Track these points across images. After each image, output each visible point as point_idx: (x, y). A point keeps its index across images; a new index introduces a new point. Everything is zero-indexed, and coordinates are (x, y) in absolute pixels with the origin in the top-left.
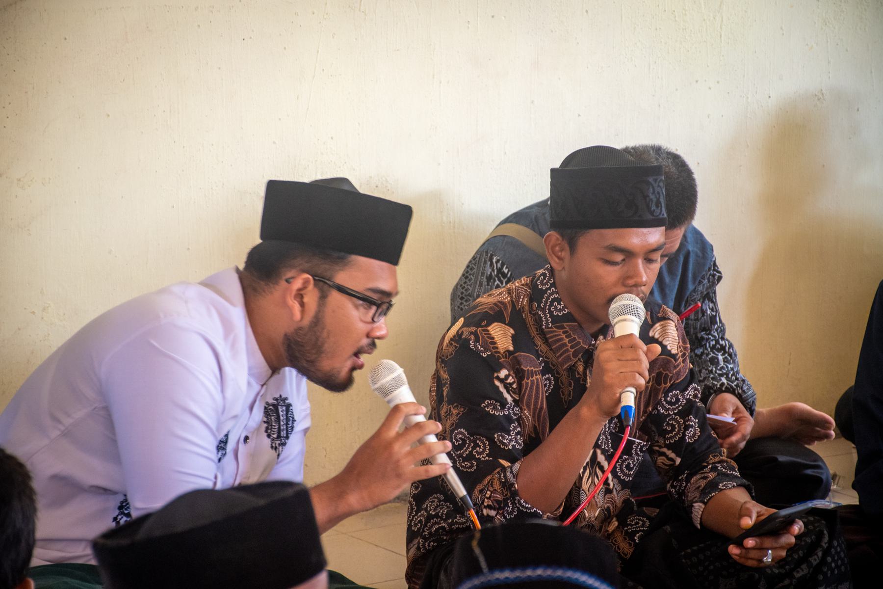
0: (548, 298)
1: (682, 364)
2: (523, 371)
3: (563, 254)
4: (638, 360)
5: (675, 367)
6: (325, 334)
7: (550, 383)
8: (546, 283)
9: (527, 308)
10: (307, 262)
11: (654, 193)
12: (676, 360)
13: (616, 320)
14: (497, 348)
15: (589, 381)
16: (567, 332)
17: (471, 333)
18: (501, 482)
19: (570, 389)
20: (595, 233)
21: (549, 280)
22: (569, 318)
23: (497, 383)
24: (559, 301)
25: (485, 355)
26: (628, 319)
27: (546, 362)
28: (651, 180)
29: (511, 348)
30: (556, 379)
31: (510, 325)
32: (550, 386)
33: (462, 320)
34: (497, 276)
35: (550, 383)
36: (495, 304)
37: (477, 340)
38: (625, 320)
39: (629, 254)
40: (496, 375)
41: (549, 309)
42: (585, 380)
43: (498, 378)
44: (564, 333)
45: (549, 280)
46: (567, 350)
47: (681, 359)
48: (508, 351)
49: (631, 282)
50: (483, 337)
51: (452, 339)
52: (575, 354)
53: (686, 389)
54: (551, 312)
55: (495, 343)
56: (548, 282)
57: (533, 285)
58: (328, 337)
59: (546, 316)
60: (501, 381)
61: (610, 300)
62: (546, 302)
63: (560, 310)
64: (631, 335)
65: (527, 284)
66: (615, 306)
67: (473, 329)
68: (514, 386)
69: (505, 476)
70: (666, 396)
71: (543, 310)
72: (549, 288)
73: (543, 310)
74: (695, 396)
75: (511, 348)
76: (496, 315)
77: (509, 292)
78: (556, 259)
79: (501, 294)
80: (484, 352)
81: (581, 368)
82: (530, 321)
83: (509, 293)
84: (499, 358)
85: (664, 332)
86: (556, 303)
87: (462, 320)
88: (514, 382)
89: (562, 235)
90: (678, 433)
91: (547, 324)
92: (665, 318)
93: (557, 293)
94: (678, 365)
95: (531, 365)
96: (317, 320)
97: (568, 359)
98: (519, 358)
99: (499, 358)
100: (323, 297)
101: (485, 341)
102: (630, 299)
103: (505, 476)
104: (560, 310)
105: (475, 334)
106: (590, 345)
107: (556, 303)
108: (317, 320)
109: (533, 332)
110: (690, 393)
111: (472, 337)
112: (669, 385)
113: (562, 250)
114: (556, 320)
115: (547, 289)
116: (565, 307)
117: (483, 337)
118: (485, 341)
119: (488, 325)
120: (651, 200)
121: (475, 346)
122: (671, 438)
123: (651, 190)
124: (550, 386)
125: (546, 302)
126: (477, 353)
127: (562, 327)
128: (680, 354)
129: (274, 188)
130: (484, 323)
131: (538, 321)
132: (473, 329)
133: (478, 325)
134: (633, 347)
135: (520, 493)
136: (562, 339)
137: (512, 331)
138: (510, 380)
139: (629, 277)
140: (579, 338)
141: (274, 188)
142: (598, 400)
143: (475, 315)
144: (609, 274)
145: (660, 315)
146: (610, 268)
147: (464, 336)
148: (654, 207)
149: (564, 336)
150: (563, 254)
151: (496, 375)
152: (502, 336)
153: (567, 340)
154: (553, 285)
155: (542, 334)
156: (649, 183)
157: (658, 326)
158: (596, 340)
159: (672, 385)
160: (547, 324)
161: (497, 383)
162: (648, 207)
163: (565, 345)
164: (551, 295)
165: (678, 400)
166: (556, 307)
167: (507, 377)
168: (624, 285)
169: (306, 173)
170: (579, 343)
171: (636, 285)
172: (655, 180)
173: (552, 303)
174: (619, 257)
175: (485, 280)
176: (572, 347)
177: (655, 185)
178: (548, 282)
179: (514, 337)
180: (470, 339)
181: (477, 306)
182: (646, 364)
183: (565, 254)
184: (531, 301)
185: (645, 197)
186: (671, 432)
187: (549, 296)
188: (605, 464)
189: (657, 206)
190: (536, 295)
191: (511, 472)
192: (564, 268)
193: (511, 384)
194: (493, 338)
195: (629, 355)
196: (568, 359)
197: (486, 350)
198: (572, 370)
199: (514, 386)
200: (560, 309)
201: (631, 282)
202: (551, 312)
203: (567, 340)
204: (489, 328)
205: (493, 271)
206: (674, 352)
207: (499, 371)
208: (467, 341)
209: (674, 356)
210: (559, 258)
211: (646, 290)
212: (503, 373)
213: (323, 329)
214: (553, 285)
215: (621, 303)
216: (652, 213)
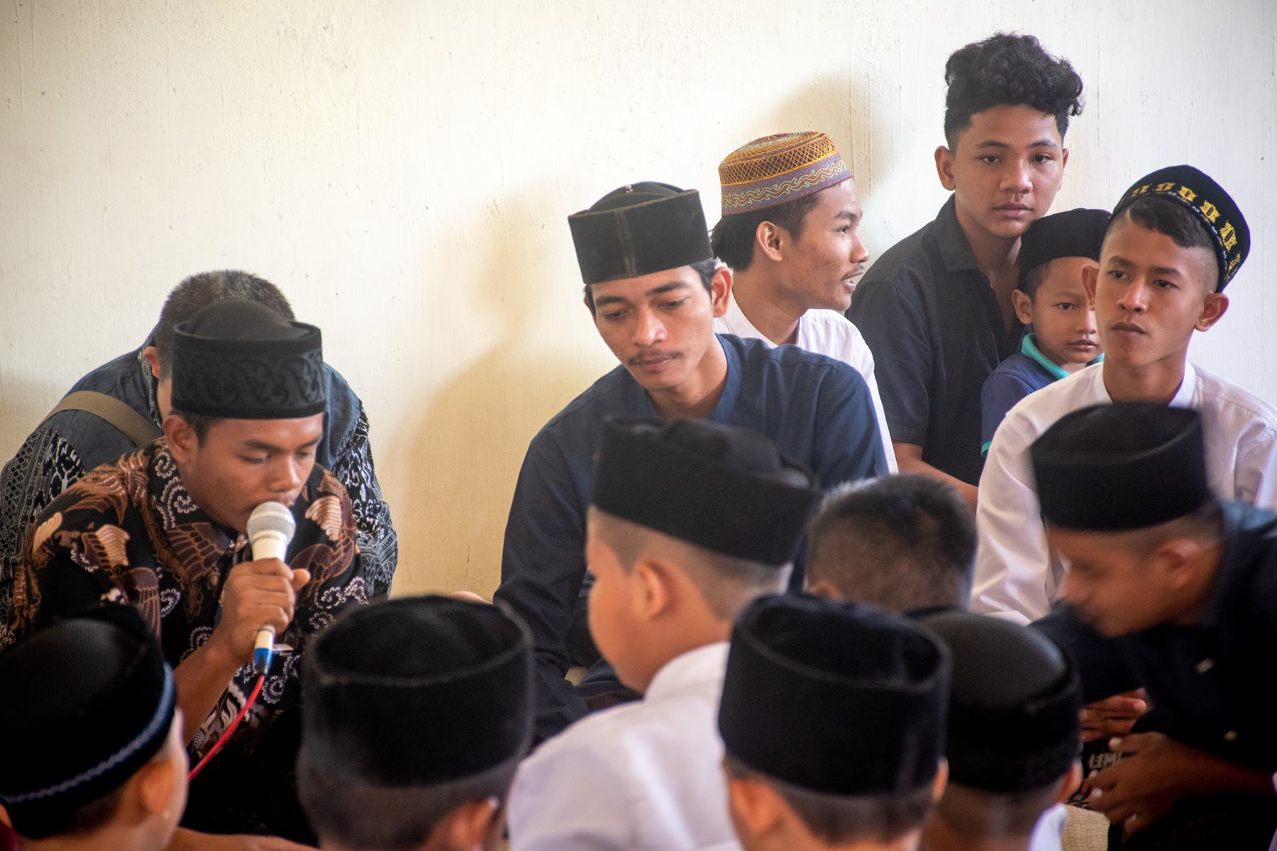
0: (170, 490)
2: (137, 592)
4: (283, 591)
5: (334, 558)
8: (167, 471)
9: (144, 503)
11: (309, 372)
12: (335, 549)
13: (255, 537)
14: (107, 561)
15: (223, 596)
17: (73, 540)
20: (232, 424)
21: (171, 466)
25: (91, 570)
26: (272, 537)
28: (306, 356)
29: (126, 563)
31: (124, 527)
34: (58, 465)
36: (105, 499)
37: (81, 549)
38: (268, 537)
39: (275, 452)
40: (103, 597)
41: (172, 505)
44: (193, 535)
45: (171, 466)
46: (197, 558)
47: (343, 547)
48: (122, 566)
49: (276, 485)
53: (347, 584)
54: (174, 510)
55: (105, 555)
61: (251, 508)
62: (168, 495)
63: (186, 507)
64: (274, 560)
66: (255, 517)
67: (76, 534)
70: (321, 594)
71: (164, 505)
72: (171, 478)
73: (164, 505)
74: (358, 592)
75: (126, 563)
76: (107, 514)
77: (123, 479)
79: (112, 482)
80: (90, 565)
81: (215, 580)
82: (149, 519)
83: (123, 484)
84: (110, 574)
85: (324, 512)
86: (180, 498)
89: (189, 421)
91: (170, 524)
92: (327, 493)
93: (181, 484)
95: (148, 579)
99: (110, 574)
101: (91, 551)
102: (278, 510)
104: (186, 507)
105: (79, 541)
106: (229, 549)
107: (180, 498)
109: (152, 534)
110: (352, 588)
111: (74, 545)
112: (322, 580)
113: (187, 438)
114: (181, 519)
115: (168, 479)
118: (91, 551)
119: (96, 528)
120: (306, 383)
121: (78, 557)
123: (306, 369)
126: (79, 568)
127: (190, 528)
130: (91, 526)
131: (159, 519)
134: (276, 573)
137: (126, 536)
139: (275, 480)
142: (230, 641)
144: (250, 475)
145: (320, 489)
146: (252, 468)
148: (308, 391)
149: (192, 540)
152: (110, 538)
153: (196, 545)
154: (176, 473)
155: (163, 535)
156: (303, 362)
157: (317, 504)
159: (327, 582)
160: (170, 524)
162: (303, 394)
163: (193, 551)
164: (174, 486)
165: (336, 599)
166: (180, 503)
168: (269, 490)
171: (284, 490)
172: (311, 356)
173: (175, 499)
174: (263, 455)
177: (311, 362)
179: (128, 544)
180: (71, 549)
182: (292, 598)
183: (192, 443)
184: (149, 494)
185: (298, 379)
188: (240, 696)
189: (313, 389)
192: (189, 461)
194: (102, 548)
195: (272, 582)
196: (198, 568)
197: (93, 563)
198: (204, 581)
200: (186, 506)
201: (276, 485)
202: (174, 510)
206: (335, 538)
207: (108, 591)
209: (332, 544)
210: (183, 447)
211: (293, 494)
214: (176, 473)
215: (264, 514)
216: (306, 398)
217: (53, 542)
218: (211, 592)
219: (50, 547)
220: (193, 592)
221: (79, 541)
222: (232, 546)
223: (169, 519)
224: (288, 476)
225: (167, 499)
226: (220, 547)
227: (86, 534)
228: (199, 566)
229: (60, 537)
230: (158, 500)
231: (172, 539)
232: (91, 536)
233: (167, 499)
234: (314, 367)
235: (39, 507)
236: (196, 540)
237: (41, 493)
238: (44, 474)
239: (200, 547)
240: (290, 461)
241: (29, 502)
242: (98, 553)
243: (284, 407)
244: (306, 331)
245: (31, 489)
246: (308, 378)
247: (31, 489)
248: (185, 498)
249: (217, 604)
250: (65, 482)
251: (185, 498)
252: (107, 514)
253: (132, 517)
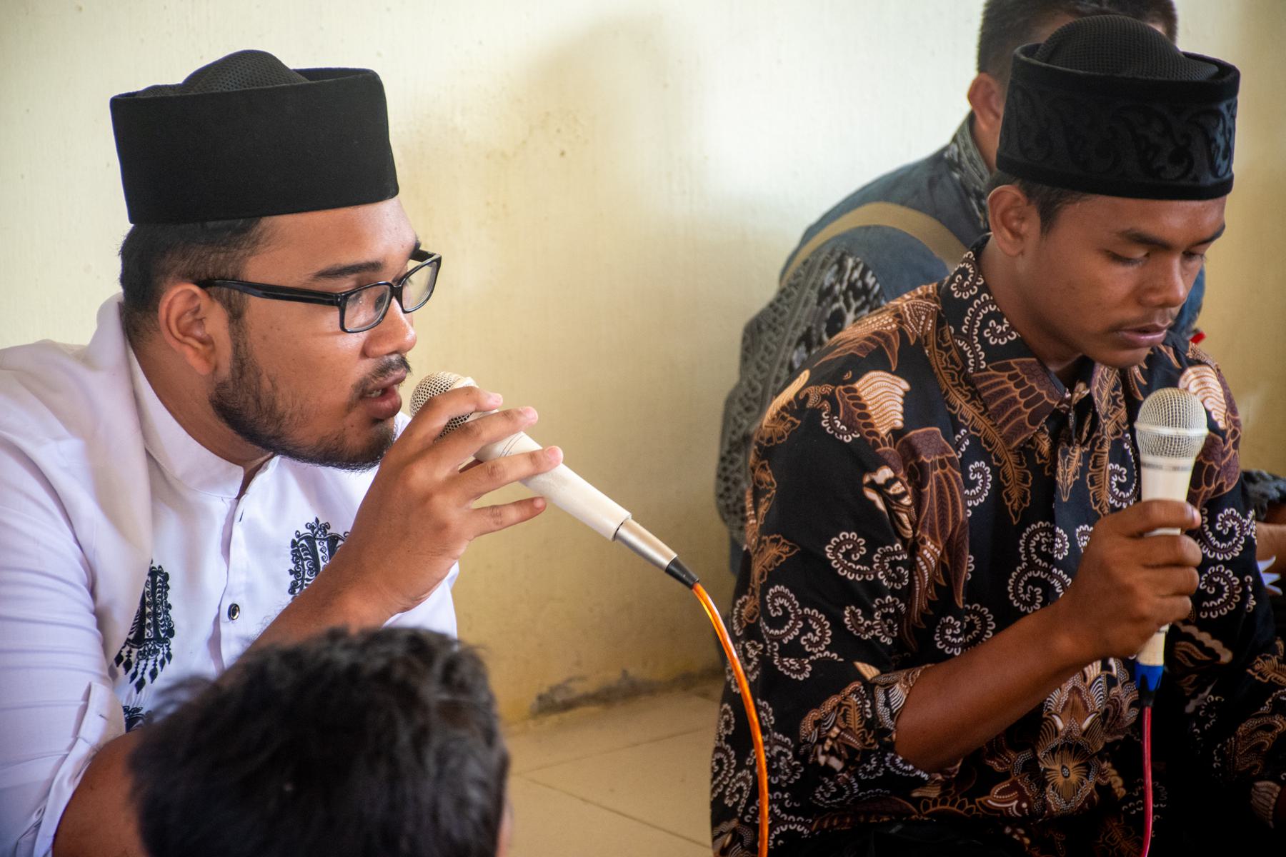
0: (975, 314)
1: (1232, 451)
3: (1024, 228)
6: (266, 384)
7: (985, 478)
8: (970, 287)
9: (932, 338)
10: (184, 257)
16: (1017, 376)
18: (863, 717)
19: (1025, 486)
21: (975, 280)
22: (1020, 348)
23: (871, 495)
24: (998, 317)
25: (848, 439)
27: (972, 438)
30: (995, 471)
32: (984, 484)
33: (805, 376)
34: (845, 293)
35: (985, 478)
36: (868, 339)
37: (834, 411)
40: (867, 479)
41: (980, 335)
42: (1053, 469)
43: (873, 485)
44: (1011, 378)
45: (975, 280)
46: (1018, 412)
47: (1231, 441)
50: (846, 405)
51: (783, 408)
52: (1034, 419)
54: (983, 341)
55: (868, 416)
56: (973, 283)
57: (944, 296)
58: (275, 388)
59: (973, 348)
60: (879, 489)
62: (972, 323)
65: (928, 296)
67: (827, 389)
68: (906, 501)
69: (873, 708)
71: (968, 338)
72: (978, 296)
76: (873, 356)
78: (1008, 235)
81: (1045, 446)
82: (938, 361)
86: (992, 323)
87: (805, 376)
88: (904, 494)
89: (1029, 194)
90: (1227, 602)
91: (977, 363)
93: (993, 303)
94: (1228, 451)
96: (242, 363)
97: (1021, 427)
98: (915, 441)
99: (876, 445)
100: (236, 316)
103: (873, 708)
105: (831, 398)
108: (242, 363)
109: (946, 381)
111: (826, 404)
113: (1022, 219)
114: (993, 354)
115: (972, 298)
116: (1012, 328)
117: (846, 405)
118: (849, 413)
119: (856, 378)
121: (831, 423)
122: (1213, 609)
124: (984, 484)
125: (972, 323)
127: (1007, 367)
128: (1230, 431)
129: (129, 112)
130: (848, 376)
132: (827, 389)
133: (836, 379)
135: (897, 748)
136: (1007, 390)
137: (906, 386)
138: (897, 488)
139: (1153, 290)
140: (1041, 387)
141: (129, 112)
143: (830, 363)
146: (1120, 270)
147: (809, 405)
148: (1219, 160)
149: (1011, 384)
150: (1024, 228)
151: (867, 479)
152: (884, 396)
153: (1016, 392)
154: (985, 288)
158: (1072, 392)
160: (977, 363)
161: (871, 495)
163: (1013, 401)
166: (993, 330)
167: (889, 482)
169: (171, 68)
170: (1040, 397)
174: (1139, 253)
175: (814, 296)
176: (1027, 405)
178: (973, 283)
179: (907, 396)
181: (835, 347)
183: (1031, 227)
184: (940, 323)
185: (1210, 141)
186: (1215, 597)
187: (975, 314)
190: (950, 310)
191: (887, 704)
192: (1022, 253)
193: (898, 497)
194: (864, 406)
196: (1021, 427)
197: (851, 429)
199: (906, 501)
200: (1001, 334)
201: (1155, 298)
202: (983, 341)
203: (1016, 392)
204: (857, 385)
205: (841, 282)
207: (874, 470)
208: (816, 413)
212: (884, 474)
213: (258, 375)
214: (985, 288)
217: (798, 406)
218: (1043, 465)
219: (793, 413)
220: (1011, 469)
221: (831, 398)
222: (1068, 396)
223: (976, 357)
224: (1172, 287)
225: (970, 329)
226: (1051, 395)
227: (841, 387)
228: (1022, 423)
229: (807, 396)
230: (958, 331)
231: (980, 386)
232: (847, 391)
233: (970, 329)
234: (1228, 124)
235: (802, 348)
236: (1017, 386)
237: (809, 329)
238: (819, 303)
239: (1022, 395)
240: (1176, 262)
241: (789, 344)
242: (859, 415)
243: (1183, 182)
244: (1216, 69)
245: (797, 324)
246: (1221, 141)
247: (797, 324)
248: (1000, 323)
249: (1055, 483)
250: (850, 317)
251: (1000, 323)
252: (873, 356)
253: (908, 358)
